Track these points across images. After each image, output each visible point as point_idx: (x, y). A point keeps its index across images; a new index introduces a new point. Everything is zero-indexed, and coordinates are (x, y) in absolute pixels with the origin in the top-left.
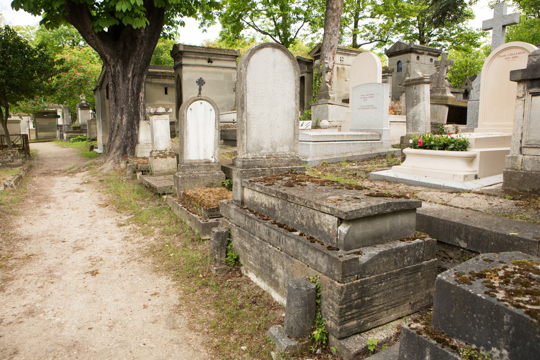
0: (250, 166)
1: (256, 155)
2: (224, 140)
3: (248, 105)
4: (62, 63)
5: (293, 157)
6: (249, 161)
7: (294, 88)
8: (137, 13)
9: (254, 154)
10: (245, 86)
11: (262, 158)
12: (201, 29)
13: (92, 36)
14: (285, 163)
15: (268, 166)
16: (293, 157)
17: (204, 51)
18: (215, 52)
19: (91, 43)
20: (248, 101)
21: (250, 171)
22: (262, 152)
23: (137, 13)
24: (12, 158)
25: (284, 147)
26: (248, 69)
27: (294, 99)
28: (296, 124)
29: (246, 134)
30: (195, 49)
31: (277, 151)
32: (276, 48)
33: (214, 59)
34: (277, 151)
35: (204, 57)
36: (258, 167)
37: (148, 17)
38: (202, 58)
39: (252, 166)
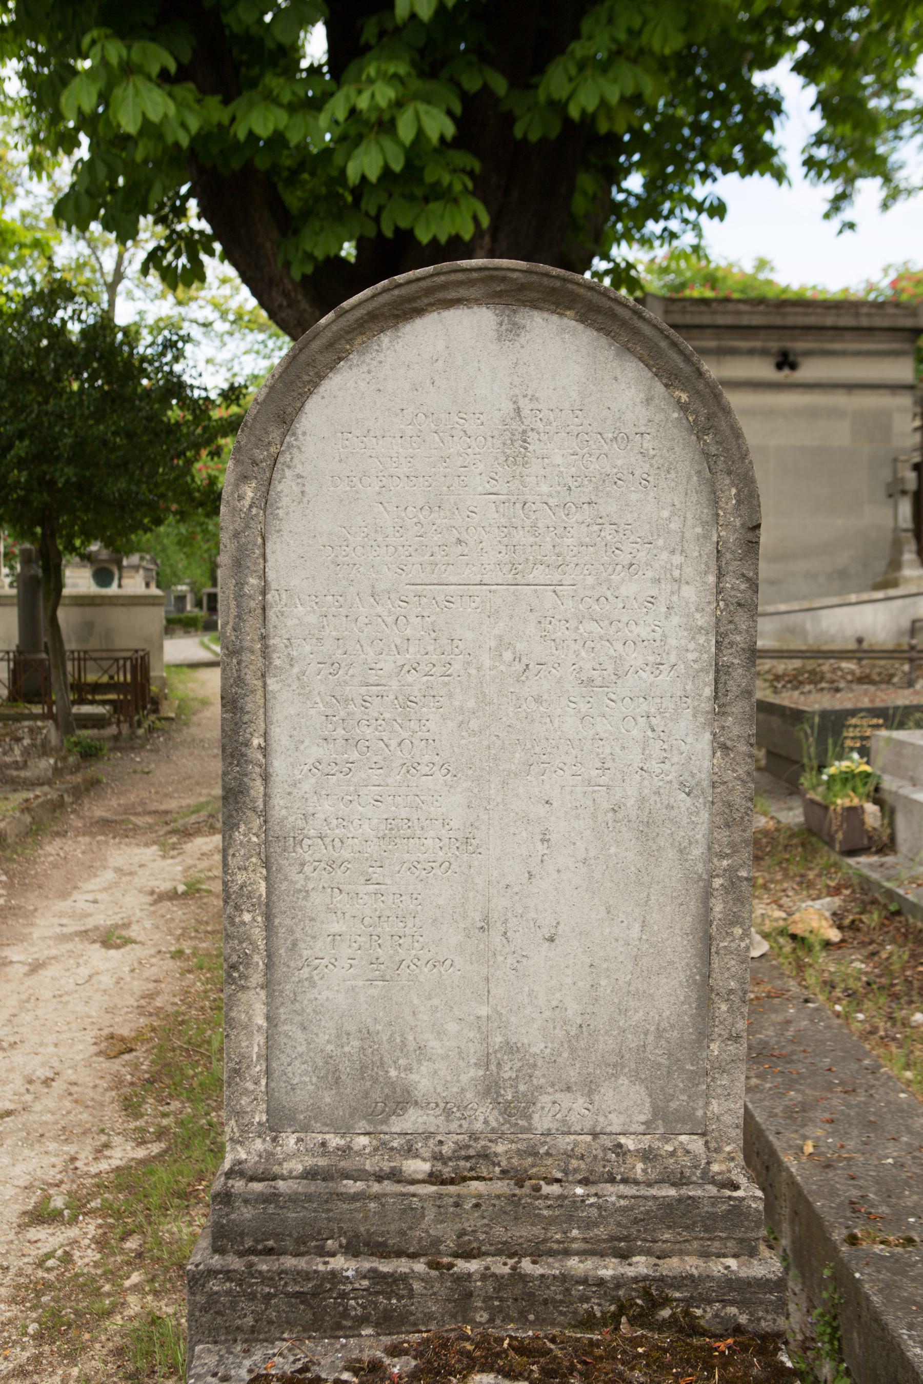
0: (276, 1236)
1: (346, 1151)
2: (769, 753)
3: (279, 765)
4: (238, 399)
5: (680, 1181)
6: (271, 1198)
7: (703, 620)
8: (438, 183)
9: (335, 1141)
10: (251, 624)
11: (395, 1176)
12: (836, 222)
13: (286, 295)
14: (600, 1232)
15: (436, 1242)
16: (680, 1181)
17: (757, 320)
18: (811, 320)
19: (283, 320)
20: (280, 735)
21: (265, 1278)
22: (397, 1125)
23: (438, 183)
24: (26, 752)
25: (607, 1096)
26: (286, 487)
27: (706, 706)
28: (718, 907)
29: (268, 985)
30: (714, 313)
31: (542, 1121)
32: (534, 305)
33: (809, 353)
34: (542, 1121)
35: (758, 344)
36: (352, 1251)
37: (481, 190)
38: (751, 352)
39: (301, 1241)
